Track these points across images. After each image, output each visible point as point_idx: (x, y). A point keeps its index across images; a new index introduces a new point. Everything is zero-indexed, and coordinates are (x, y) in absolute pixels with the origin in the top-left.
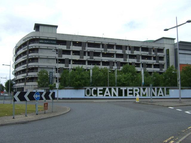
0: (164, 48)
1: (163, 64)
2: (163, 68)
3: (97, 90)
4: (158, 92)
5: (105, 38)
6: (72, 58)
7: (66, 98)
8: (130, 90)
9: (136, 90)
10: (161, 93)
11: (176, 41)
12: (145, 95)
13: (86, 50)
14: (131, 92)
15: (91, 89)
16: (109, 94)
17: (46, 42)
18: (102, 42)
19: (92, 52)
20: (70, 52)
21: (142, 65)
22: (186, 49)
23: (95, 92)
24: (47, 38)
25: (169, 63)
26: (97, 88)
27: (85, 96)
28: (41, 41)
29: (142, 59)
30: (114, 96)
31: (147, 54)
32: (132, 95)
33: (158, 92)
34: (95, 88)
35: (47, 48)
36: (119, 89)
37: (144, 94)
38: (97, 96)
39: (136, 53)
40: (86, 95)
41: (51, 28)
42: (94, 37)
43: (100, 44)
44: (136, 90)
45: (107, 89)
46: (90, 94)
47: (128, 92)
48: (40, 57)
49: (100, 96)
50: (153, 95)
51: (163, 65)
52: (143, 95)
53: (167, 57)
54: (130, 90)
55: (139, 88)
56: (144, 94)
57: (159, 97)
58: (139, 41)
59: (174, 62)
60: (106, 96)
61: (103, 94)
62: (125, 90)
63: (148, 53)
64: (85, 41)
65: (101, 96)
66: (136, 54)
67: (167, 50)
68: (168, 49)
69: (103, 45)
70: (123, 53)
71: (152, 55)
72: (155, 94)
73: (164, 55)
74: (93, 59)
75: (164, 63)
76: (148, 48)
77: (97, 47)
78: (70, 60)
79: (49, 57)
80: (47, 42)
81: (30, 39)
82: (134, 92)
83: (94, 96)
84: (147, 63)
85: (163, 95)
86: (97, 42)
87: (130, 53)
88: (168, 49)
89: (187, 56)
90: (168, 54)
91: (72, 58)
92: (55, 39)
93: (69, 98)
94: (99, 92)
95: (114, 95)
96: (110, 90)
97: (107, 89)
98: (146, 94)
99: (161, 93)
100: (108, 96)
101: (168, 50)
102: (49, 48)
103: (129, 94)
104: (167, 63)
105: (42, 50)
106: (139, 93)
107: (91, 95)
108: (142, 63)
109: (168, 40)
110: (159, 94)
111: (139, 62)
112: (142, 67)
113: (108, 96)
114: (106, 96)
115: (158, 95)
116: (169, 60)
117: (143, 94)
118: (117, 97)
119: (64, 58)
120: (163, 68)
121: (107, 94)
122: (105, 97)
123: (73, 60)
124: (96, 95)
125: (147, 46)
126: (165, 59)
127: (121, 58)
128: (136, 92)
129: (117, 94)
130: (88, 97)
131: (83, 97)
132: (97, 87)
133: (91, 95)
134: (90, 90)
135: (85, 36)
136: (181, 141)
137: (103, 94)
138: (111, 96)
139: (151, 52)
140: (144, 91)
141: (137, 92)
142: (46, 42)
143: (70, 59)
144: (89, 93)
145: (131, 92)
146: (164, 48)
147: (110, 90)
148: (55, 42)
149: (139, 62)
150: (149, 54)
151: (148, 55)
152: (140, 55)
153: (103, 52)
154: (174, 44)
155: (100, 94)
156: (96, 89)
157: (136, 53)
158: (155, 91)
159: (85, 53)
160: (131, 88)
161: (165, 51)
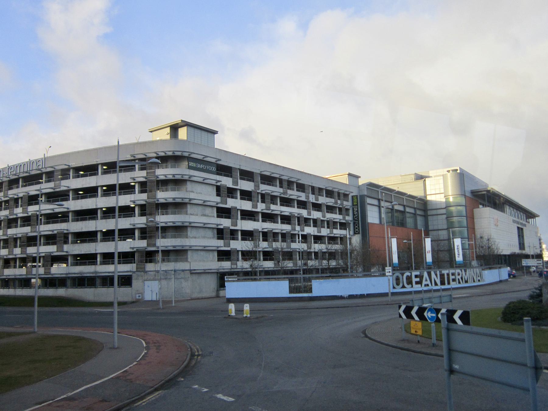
3: (411, 275)
7: (357, 295)
8: (416, 276)
11: (361, 182)
15: (403, 274)
16: (429, 282)
21: (328, 224)
22: (373, 196)
23: (409, 281)
27: (394, 288)
32: (420, 285)
34: (407, 274)
36: (440, 272)
38: (412, 287)
41: (206, 133)
44: (459, 274)
45: (426, 275)
46: (401, 285)
49: (417, 288)
54: (416, 276)
55: (400, 273)
59: (475, 225)
60: (425, 285)
69: (281, 181)
74: (269, 209)
76: (333, 191)
80: (202, 166)
85: (430, 285)
93: (364, 295)
94: (414, 280)
95: (436, 284)
96: (429, 274)
97: (426, 275)
99: (426, 280)
100: (428, 285)
103: (415, 283)
105: (193, 184)
107: (403, 287)
113: (428, 285)
114: (425, 285)
118: (439, 287)
124: (410, 286)
129: (438, 282)
130: (399, 290)
133: (403, 287)
134: (400, 276)
136: (142, 396)
138: (432, 285)
147: (429, 274)
155: (417, 283)
156: (409, 274)
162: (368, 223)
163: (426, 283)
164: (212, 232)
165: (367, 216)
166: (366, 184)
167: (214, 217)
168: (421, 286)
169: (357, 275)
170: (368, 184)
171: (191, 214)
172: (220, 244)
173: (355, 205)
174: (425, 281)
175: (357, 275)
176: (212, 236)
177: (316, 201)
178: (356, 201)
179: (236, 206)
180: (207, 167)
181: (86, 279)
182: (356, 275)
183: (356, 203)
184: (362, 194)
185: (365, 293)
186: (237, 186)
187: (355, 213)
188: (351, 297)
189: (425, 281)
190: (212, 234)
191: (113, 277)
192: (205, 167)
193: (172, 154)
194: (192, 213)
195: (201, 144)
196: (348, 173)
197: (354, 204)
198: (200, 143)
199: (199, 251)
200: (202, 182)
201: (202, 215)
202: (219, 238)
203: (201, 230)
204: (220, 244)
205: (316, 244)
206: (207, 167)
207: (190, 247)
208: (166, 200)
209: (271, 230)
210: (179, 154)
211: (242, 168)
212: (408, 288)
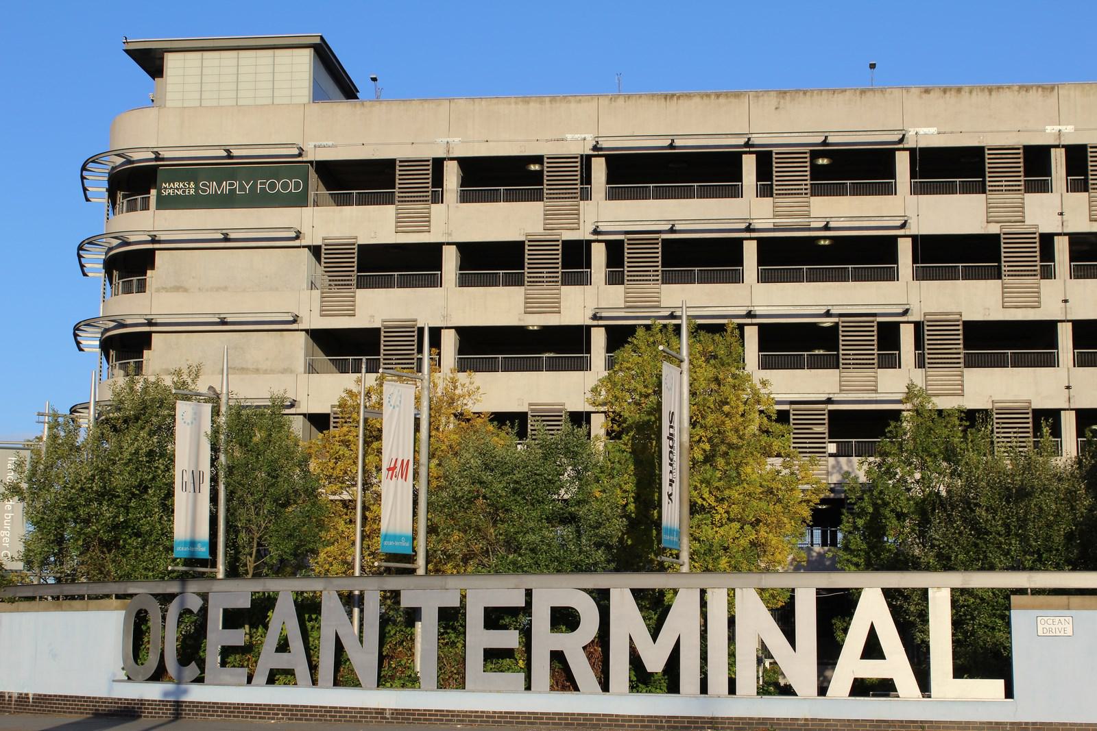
4: (828, 652)
8: (495, 618)
9: (565, 619)
10: (873, 649)
12: (671, 679)
13: (584, 234)
14: (509, 639)
16: (296, 659)
28: (170, 189)
30: (633, 688)
33: (828, 652)
44: (565, 619)
47: (478, 638)
50: (774, 685)
52: (641, 679)
55: (590, 592)
56: (655, 661)
60: (861, 688)
70: (994, 229)
82: (545, 640)
85: (302, 670)
99: (873, 649)
100: (885, 688)
101: (330, 281)
106: (600, 649)
110: (851, 665)
112: (920, 363)
113: (885, 688)
114: (861, 688)
117: (636, 661)
121: (873, 670)
127: (970, 275)
140: (655, 637)
141: (574, 644)
145: (509, 639)
160: (507, 593)
174: (278, 650)
180: (254, 187)
189: (278, 650)
192: (242, 188)
206: (254, 187)
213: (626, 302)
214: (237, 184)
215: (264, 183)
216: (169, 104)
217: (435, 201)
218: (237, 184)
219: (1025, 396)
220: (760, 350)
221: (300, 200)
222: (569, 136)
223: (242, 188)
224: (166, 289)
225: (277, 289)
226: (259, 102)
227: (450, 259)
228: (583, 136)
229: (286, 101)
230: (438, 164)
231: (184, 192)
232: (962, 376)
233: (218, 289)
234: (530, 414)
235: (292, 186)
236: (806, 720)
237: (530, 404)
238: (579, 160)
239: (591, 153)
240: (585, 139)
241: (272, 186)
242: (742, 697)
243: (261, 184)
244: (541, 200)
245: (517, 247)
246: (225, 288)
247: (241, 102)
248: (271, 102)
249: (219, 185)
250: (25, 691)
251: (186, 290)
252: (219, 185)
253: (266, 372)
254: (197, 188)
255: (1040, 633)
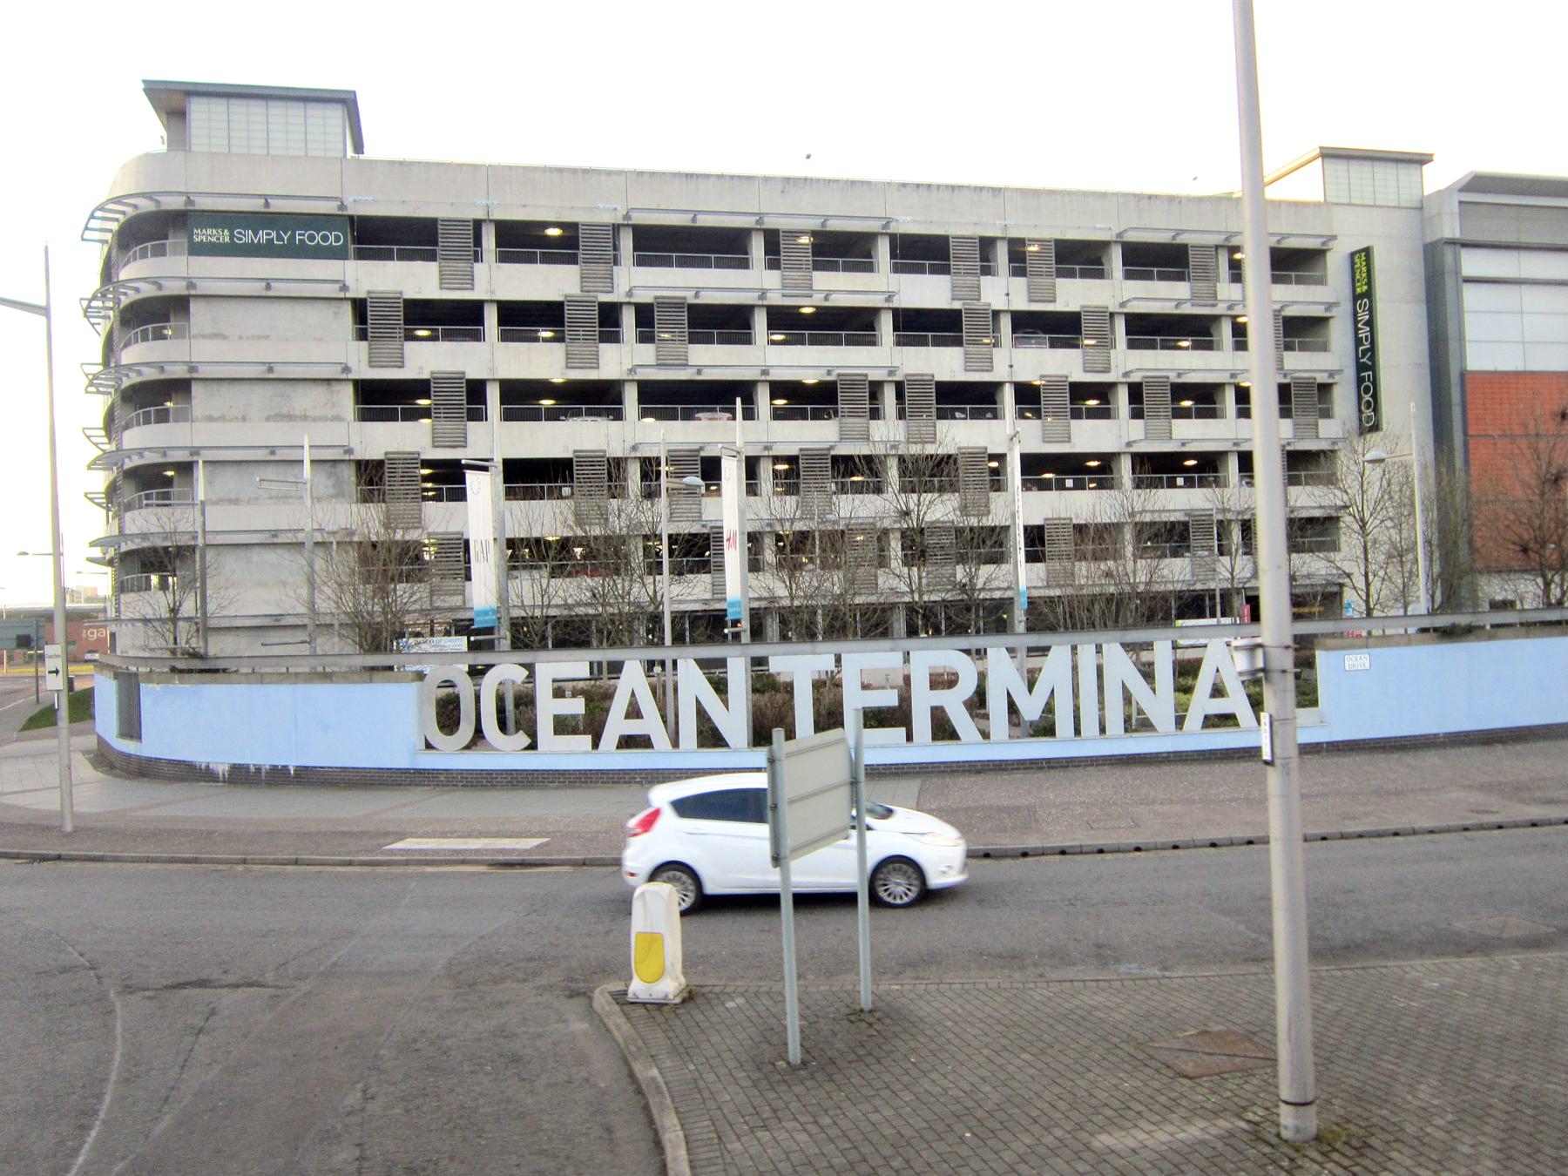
0: (1334, 238)
1: (1322, 378)
2: (1326, 414)
5: (787, 180)
6: (492, 370)
9: (943, 681)
11: (1438, 178)
12: (1045, 728)
16: (650, 723)
17: (248, 237)
18: (761, 216)
19: (676, 305)
20: (479, 320)
22: (1526, 239)
24: (256, 205)
25: (1373, 367)
26: (530, 667)
28: (203, 235)
29: (1132, 345)
30: (935, 737)
31: (1179, 303)
35: (258, 289)
37: (1031, 710)
38: (533, 746)
39: (1072, 295)
40: (437, 737)
42: (689, 176)
43: (869, 238)
46: (466, 731)
48: (204, 372)
49: (572, 753)
50: (1138, 723)
51: (1325, 389)
53: (1356, 322)
57: (1197, 738)
58: (1103, 195)
60: (628, 742)
61: (593, 725)
62: (818, 686)
63: (1181, 289)
64: (608, 218)
65: (572, 753)
66: (1073, 307)
67: (1360, 262)
68: (1367, 252)
69: (773, 241)
70: (957, 305)
71: (1220, 309)
72: (1159, 702)
73: (1329, 306)
75: (1331, 374)
77: (849, 268)
78: (476, 390)
79: (280, 372)
80: (263, 236)
81: (130, 212)
82: (923, 702)
83: (506, 752)
84: (1174, 378)
85: (660, 737)
86: (716, 213)
87: (1021, 304)
88: (1367, 252)
89: (1530, 296)
90: (1363, 297)
91: (492, 370)
92: (329, 208)
94: (547, 708)
98: (1049, 709)
99: (634, 712)
100: (1228, 720)
101: (1362, 259)
102: (279, 289)
104: (1360, 367)
106: (978, 703)
108: (1135, 378)
109: (1381, 170)
110: (1202, 703)
111: (1107, 370)
112: (901, 415)
113: (1228, 720)
114: (628, 742)
115: (1194, 720)
116: (1373, 349)
117: (1012, 708)
119: (426, 376)
120: (1326, 414)
122: (610, 757)
123: (778, 389)
125: (1179, 232)
126: (1340, 334)
128: (943, 698)
129: (734, 720)
130: (451, 755)
131: (400, 752)
132: (527, 656)
135: (609, 173)
137: (593, 725)
138: (675, 743)
139: (1217, 279)
141: (954, 701)
142: (248, 237)
143: (474, 373)
144: (458, 723)
146: (1334, 238)
148: (334, 238)
149: (1107, 370)
150: (1195, 298)
151: (1187, 309)
152: (1112, 315)
153: (776, 299)
154: (1420, 209)
155: (563, 726)
157: (1072, 295)
158: (701, 713)
159: (609, 316)
161: (1336, 263)
162: (1464, 375)
163: (634, 728)
164: (329, 477)
165: (1461, 338)
166: (1460, 186)
167: (338, 418)
168: (595, 745)
169: (291, 670)
170: (1463, 183)
171: (210, 419)
172: (367, 520)
173: (1362, 296)
174: (628, 716)
175: (1388, 632)
176: (331, 491)
177: (1031, 301)
178: (1364, 275)
179: (461, 369)
180: (292, 238)
181: (820, 611)
182: (1406, 631)
183: (1365, 288)
184: (1434, 239)
185: (292, 762)
186: (612, 292)
187: (1362, 335)
188: (241, 776)
189: (628, 716)
190: (330, 483)
191: (721, 613)
192: (280, 238)
193: (186, 206)
194: (216, 415)
195: (307, 155)
196: (1318, 151)
197: (1359, 290)
198: (302, 153)
199: (257, 550)
200: (264, 293)
201: (268, 419)
202: (366, 498)
203: (259, 474)
204: (367, 520)
205: (1296, 488)
206: (292, 238)
207: (274, 536)
208: (162, 369)
209: (696, 451)
210: (175, 204)
211: (640, 219)
212: (506, 752)
213: (658, 359)
214: (274, 234)
215: (303, 235)
216: (194, 148)
217: (476, 260)
218: (274, 234)
219: (982, 444)
220: (502, 403)
221: (338, 254)
222: (601, 206)
223: (280, 238)
224: (204, 337)
225: (321, 339)
226: (291, 153)
227: (491, 316)
228: (613, 206)
229: (320, 154)
230: (478, 224)
231: (218, 239)
232: (1069, 426)
233: (259, 337)
234: (575, 459)
235: (332, 238)
236: (1168, 753)
237: (575, 451)
238: (611, 228)
239: (621, 222)
240: (615, 209)
241: (312, 238)
242: (1086, 739)
243: (299, 235)
244: (576, 263)
245: (559, 306)
246: (267, 337)
247: (273, 152)
248: (302, 153)
249: (256, 234)
250: (280, 762)
251: (225, 337)
252: (256, 234)
253: (315, 419)
254: (232, 236)
255: (1347, 668)
